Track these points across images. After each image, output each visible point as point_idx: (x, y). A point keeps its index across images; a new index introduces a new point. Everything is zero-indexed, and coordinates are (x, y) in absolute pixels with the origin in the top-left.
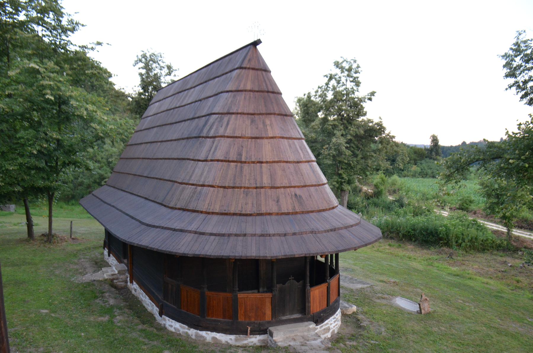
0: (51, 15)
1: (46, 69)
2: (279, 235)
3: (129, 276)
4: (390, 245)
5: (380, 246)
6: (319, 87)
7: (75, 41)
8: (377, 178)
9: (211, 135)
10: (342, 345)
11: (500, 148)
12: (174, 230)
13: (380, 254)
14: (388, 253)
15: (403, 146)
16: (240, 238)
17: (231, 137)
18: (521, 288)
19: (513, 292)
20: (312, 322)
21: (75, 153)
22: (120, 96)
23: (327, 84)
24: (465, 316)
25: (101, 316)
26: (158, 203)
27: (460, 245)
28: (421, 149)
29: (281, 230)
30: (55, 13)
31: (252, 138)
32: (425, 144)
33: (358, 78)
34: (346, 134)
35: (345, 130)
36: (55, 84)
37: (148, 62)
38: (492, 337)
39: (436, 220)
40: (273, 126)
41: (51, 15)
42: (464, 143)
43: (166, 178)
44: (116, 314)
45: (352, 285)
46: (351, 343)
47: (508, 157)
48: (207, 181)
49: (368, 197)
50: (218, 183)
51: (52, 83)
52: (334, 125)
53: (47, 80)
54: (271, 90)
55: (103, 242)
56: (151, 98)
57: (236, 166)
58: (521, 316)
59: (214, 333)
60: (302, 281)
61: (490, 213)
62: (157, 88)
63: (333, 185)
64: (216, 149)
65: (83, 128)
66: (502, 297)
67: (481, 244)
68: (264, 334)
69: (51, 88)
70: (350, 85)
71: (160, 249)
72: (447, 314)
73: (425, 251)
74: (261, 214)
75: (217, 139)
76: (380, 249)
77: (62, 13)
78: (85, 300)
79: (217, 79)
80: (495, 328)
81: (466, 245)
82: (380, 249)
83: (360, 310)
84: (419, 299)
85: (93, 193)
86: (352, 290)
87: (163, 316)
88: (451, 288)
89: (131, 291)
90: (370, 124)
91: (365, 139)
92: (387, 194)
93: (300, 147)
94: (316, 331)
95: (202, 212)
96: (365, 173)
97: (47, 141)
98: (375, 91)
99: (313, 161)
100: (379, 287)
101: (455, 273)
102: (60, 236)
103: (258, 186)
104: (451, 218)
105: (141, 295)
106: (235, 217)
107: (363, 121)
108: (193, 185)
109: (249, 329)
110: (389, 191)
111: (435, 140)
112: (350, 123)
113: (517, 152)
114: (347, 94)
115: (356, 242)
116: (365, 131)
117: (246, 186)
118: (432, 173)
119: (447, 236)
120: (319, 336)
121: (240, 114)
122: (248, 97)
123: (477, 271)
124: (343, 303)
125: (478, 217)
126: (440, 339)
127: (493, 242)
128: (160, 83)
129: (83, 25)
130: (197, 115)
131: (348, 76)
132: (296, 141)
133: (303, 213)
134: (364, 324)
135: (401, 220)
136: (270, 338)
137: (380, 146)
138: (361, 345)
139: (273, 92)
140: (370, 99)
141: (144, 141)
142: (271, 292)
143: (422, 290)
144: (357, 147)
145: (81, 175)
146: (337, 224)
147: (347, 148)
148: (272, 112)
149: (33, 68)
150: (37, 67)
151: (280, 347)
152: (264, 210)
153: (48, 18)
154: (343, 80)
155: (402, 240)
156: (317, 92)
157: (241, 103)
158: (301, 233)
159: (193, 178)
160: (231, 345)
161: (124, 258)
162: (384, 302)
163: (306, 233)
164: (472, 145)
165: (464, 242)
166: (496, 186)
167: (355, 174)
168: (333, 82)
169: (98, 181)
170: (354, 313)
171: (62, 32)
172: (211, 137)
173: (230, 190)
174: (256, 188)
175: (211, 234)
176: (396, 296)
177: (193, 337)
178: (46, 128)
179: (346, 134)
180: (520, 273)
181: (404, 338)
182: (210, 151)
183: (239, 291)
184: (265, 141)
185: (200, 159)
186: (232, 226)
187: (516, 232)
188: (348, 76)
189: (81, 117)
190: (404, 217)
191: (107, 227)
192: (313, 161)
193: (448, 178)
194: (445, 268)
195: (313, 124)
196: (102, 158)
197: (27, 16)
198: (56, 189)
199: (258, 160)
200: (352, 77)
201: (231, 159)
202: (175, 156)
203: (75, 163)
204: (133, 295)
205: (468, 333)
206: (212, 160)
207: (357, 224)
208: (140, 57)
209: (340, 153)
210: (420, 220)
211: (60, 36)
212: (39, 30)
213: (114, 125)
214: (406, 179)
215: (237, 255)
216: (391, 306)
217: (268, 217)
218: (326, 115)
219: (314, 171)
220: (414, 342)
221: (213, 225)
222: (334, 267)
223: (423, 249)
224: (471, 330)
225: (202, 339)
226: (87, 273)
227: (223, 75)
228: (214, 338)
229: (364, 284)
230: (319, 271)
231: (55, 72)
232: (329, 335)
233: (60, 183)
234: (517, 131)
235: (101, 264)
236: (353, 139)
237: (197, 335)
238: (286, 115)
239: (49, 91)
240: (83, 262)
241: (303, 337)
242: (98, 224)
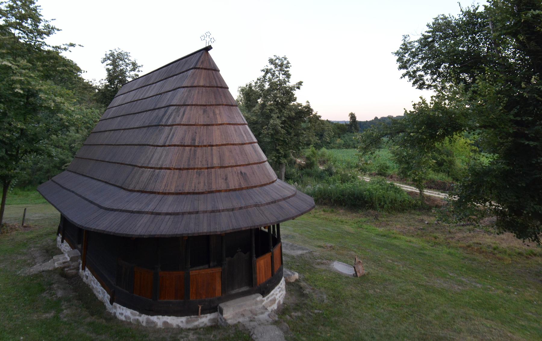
0: (29, 21)
1: (18, 66)
2: (228, 210)
3: (81, 262)
4: (324, 211)
5: (316, 212)
6: (258, 79)
7: (50, 42)
8: (308, 152)
9: (169, 124)
10: (288, 317)
11: (402, 124)
12: (132, 212)
13: (316, 220)
14: (323, 219)
15: (328, 123)
16: (193, 216)
17: (187, 125)
18: (439, 244)
19: (433, 248)
20: (259, 294)
21: (39, 141)
22: (88, 87)
23: (264, 77)
24: (395, 276)
25: (47, 312)
26: (118, 187)
27: (382, 207)
28: (343, 125)
29: (229, 205)
30: (33, 20)
31: (204, 125)
32: (346, 120)
33: (288, 71)
34: (281, 116)
35: (280, 113)
36: (26, 79)
37: (115, 60)
38: (422, 296)
39: (360, 185)
40: (222, 115)
41: (29, 21)
42: (376, 118)
43: (127, 163)
44: (63, 307)
45: (292, 251)
46: (296, 314)
47: (409, 131)
48: (165, 164)
49: (301, 168)
50: (174, 165)
51: (22, 78)
52: (271, 109)
53: (18, 76)
54: (219, 85)
55: (57, 228)
56: (116, 90)
57: (191, 149)
58: (443, 271)
59: (166, 317)
60: (246, 255)
61: (404, 177)
62: (123, 82)
63: (273, 160)
64: (173, 135)
65: (49, 116)
66: (424, 254)
67: (400, 205)
68: (214, 312)
69: (21, 82)
70: (282, 77)
71: (117, 232)
72: (380, 275)
73: (354, 214)
74: (212, 192)
75: (174, 127)
76: (317, 215)
77: (40, 20)
78: (30, 296)
79: (175, 77)
80: (422, 285)
81: (388, 206)
82: (317, 215)
83: (302, 277)
84: (354, 261)
85: (53, 178)
86: (293, 257)
87: (114, 304)
88: (380, 248)
89: (82, 279)
90: (300, 108)
91: (296, 119)
92: (319, 165)
93: (244, 131)
94: (263, 304)
95: (159, 193)
96: (298, 148)
97: (10, 131)
98: (302, 81)
99: (255, 143)
100: (318, 252)
101: (382, 234)
102: (10, 224)
103: (209, 166)
104: (372, 183)
105: (92, 283)
106: (189, 196)
107: (294, 105)
108: (151, 168)
109: (200, 308)
110: (320, 162)
111: (353, 116)
112: (284, 107)
113: (415, 127)
114: (280, 85)
115: (294, 212)
116: (296, 113)
117: (199, 167)
118: (354, 144)
119: (371, 199)
120: (266, 309)
121: (195, 105)
122: (200, 92)
123: (400, 230)
124: (286, 271)
125: (394, 180)
126: (377, 302)
127: (410, 202)
128: (125, 77)
129: (58, 30)
130: (157, 107)
131: (281, 70)
132: (240, 126)
133: (247, 188)
134: (307, 291)
135: (331, 187)
136: (220, 316)
137: (309, 125)
138: (305, 315)
139: (221, 87)
140: (298, 88)
141: (107, 129)
142: (221, 266)
143: (355, 252)
144: (290, 126)
145: (41, 161)
146: (276, 197)
147: (282, 127)
148: (221, 103)
149: (6, 65)
150: (10, 65)
151: (229, 325)
152: (214, 188)
153: (26, 23)
154: (277, 73)
155: (334, 205)
156: (256, 83)
157: (195, 97)
158: (246, 207)
159: (152, 162)
160: (182, 329)
161: (79, 244)
162: (323, 267)
163: (251, 206)
164: (383, 119)
165: (386, 204)
166: (405, 154)
167: (289, 149)
168: (269, 75)
169: (58, 165)
170: (296, 280)
171: (38, 35)
172: (169, 126)
173: (185, 171)
174: (208, 168)
175: (167, 214)
176: (334, 261)
177: (144, 324)
178: (10, 119)
179: (281, 116)
180: (436, 229)
181: (344, 304)
182: (168, 137)
183: (191, 267)
184: (215, 127)
185: (159, 144)
186: (186, 205)
187: (427, 192)
188: (281, 70)
189: (48, 108)
190: (334, 184)
191: (65, 214)
192: (255, 143)
193: (365, 150)
194: (373, 229)
195: (254, 109)
196: (65, 144)
197: (6, 21)
198: (13, 177)
199: (209, 144)
200: (284, 71)
201: (186, 144)
202: (136, 142)
203: (37, 151)
204: (84, 283)
205: (401, 294)
206: (169, 146)
207: (293, 195)
208: (109, 56)
209: (277, 132)
210: (348, 186)
211: (36, 38)
212: (16, 32)
213: (80, 115)
214: (333, 150)
215: (190, 232)
216: (330, 271)
217: (218, 194)
218: (264, 101)
219: (256, 151)
220: (353, 307)
221: (169, 205)
222: (276, 236)
223: (352, 213)
224: (403, 290)
225: (152, 325)
226: (35, 264)
227: (180, 73)
228: (165, 323)
229: (303, 250)
230: (264, 240)
231: (27, 69)
232: (275, 307)
233: (18, 170)
234: (413, 110)
235: (52, 252)
236: (287, 120)
237: (148, 322)
238: (232, 106)
239: (18, 86)
240: (33, 251)
241: (251, 312)
242: (53, 208)
